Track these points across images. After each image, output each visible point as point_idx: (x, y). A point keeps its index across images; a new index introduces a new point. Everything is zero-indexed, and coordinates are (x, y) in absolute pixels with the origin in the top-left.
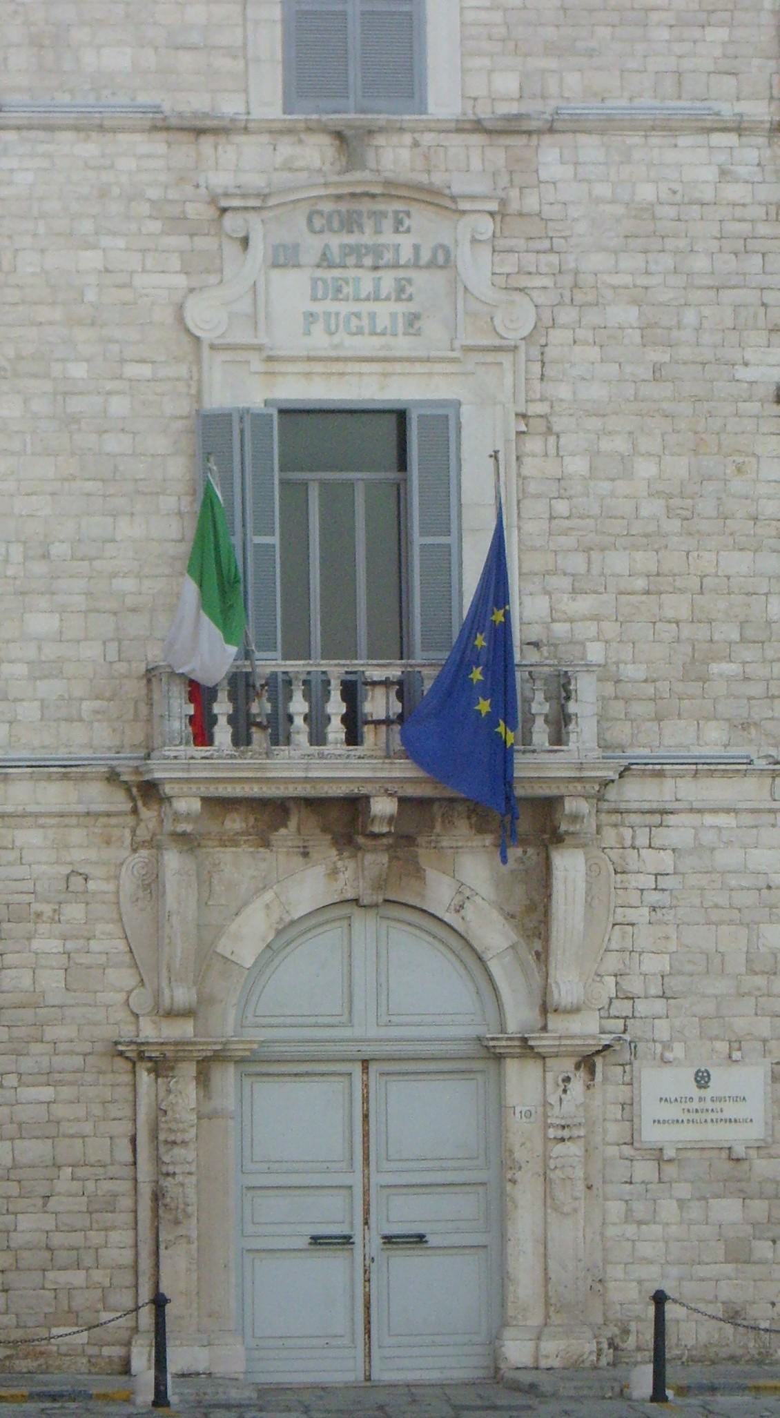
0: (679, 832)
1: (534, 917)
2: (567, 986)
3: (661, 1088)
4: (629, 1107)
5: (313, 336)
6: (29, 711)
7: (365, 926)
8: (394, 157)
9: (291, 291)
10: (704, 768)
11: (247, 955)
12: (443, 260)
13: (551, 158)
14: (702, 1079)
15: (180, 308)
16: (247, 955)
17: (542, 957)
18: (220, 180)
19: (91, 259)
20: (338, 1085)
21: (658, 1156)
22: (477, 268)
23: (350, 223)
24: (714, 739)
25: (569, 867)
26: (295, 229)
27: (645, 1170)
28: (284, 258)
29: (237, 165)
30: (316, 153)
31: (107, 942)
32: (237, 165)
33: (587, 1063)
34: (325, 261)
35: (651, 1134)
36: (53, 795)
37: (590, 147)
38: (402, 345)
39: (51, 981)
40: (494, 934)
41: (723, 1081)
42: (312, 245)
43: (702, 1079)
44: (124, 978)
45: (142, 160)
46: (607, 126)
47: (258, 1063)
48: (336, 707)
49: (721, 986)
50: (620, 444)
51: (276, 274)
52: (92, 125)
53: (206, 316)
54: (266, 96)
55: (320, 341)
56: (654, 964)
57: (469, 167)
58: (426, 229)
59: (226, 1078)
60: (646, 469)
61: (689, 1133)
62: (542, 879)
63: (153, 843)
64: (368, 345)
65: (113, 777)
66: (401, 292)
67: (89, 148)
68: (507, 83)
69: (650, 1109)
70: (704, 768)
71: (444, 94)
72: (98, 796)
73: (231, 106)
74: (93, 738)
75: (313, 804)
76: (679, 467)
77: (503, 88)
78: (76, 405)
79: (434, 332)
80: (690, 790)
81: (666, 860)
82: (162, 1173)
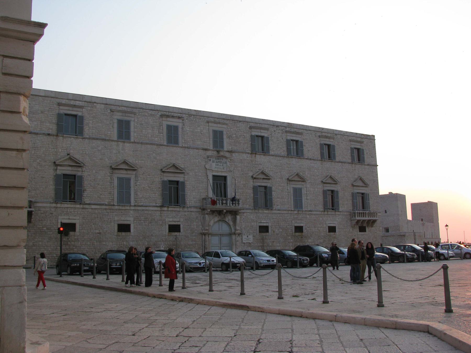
0: (245, 214)
1: (235, 221)
2: (238, 228)
3: (244, 237)
4: (242, 239)
5: (217, 168)
6: (193, 202)
7: (220, 223)
8: (222, 153)
9: (214, 165)
10: (247, 209)
11: (212, 225)
12: (226, 163)
13: (234, 154)
14: (248, 237)
15: (205, 166)
16: (212, 225)
17: (235, 226)
18: (208, 154)
19: (197, 161)
20: (218, 237)
21: (244, 243)
22: (228, 164)
23: (218, 159)
24: (247, 206)
25: (238, 217)
26: (214, 159)
27: (243, 245)
28: (213, 162)
29: (209, 153)
30: (215, 153)
31: (200, 223)
32: (209, 153)
33: (239, 235)
34: (217, 162)
35: (244, 241)
36: (195, 210)
37: (237, 154)
38: (223, 170)
39: (195, 227)
40: (231, 223)
41: (249, 237)
42: (215, 161)
43: (248, 237)
44: (201, 226)
45: (201, 152)
46: (239, 152)
47: (213, 235)
48: (221, 202)
49: (248, 228)
50: (240, 180)
51: (87, 131)
52: (197, 149)
53: (207, 167)
54: (211, 147)
55: (216, 169)
56: (244, 226)
57: (227, 155)
58: (224, 160)
59: (210, 236)
60: (242, 182)
61: (247, 241)
62: (236, 217)
63: (204, 214)
64: (220, 170)
65: (200, 208)
66: (223, 166)
67: (197, 151)
68: (230, 148)
69: (244, 239)
70: (247, 209)
71: (225, 149)
72: (199, 210)
73: (209, 148)
74: (198, 204)
75: (216, 211)
76: (244, 182)
77: (230, 148)
78: (197, 174)
79: (225, 169)
80: (246, 211)
81: (244, 217)
82: (205, 245)
